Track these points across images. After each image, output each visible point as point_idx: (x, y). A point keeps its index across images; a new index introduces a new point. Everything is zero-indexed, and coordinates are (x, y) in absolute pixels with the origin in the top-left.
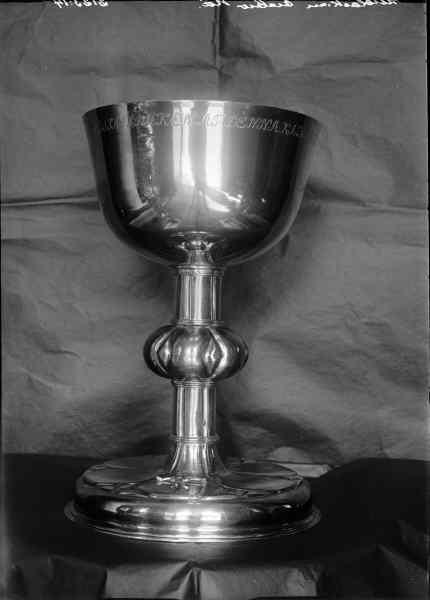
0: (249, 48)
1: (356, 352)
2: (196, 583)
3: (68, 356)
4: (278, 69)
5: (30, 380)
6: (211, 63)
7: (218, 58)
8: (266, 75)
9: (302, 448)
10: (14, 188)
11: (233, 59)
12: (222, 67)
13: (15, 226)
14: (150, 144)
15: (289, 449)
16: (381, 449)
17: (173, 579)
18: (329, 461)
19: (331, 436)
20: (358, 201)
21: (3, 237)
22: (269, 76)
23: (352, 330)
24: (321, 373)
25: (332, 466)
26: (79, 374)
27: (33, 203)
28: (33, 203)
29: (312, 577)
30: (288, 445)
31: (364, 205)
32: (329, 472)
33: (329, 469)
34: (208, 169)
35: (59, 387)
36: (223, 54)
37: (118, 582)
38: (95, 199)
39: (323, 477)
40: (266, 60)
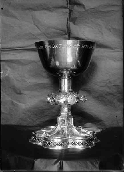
0: (78, 2)
1: (110, 94)
2: (62, 165)
3: (23, 95)
4: (87, 9)
5: (12, 102)
6: (66, 6)
7: (68, 5)
8: (82, 10)
9: (95, 124)
10: (3, 46)
11: (73, 5)
12: (70, 8)
13: (5, 56)
14: (103, 83)
15: (90, 123)
16: (118, 123)
17: (56, 161)
18: (103, 127)
19: (103, 119)
20: (110, 48)
21: (1, 60)
22: (84, 10)
23: (109, 87)
24: (100, 101)
25: (103, 129)
26: (22, 106)
27: (7, 49)
28: (7, 49)
29: (97, 163)
30: (90, 122)
31: (113, 49)
32: (102, 131)
33: (102, 130)
34: (66, 86)
35: (21, 104)
36: (70, 4)
37: (39, 164)
38: (35, 47)
39: (101, 132)
40: (83, 5)
